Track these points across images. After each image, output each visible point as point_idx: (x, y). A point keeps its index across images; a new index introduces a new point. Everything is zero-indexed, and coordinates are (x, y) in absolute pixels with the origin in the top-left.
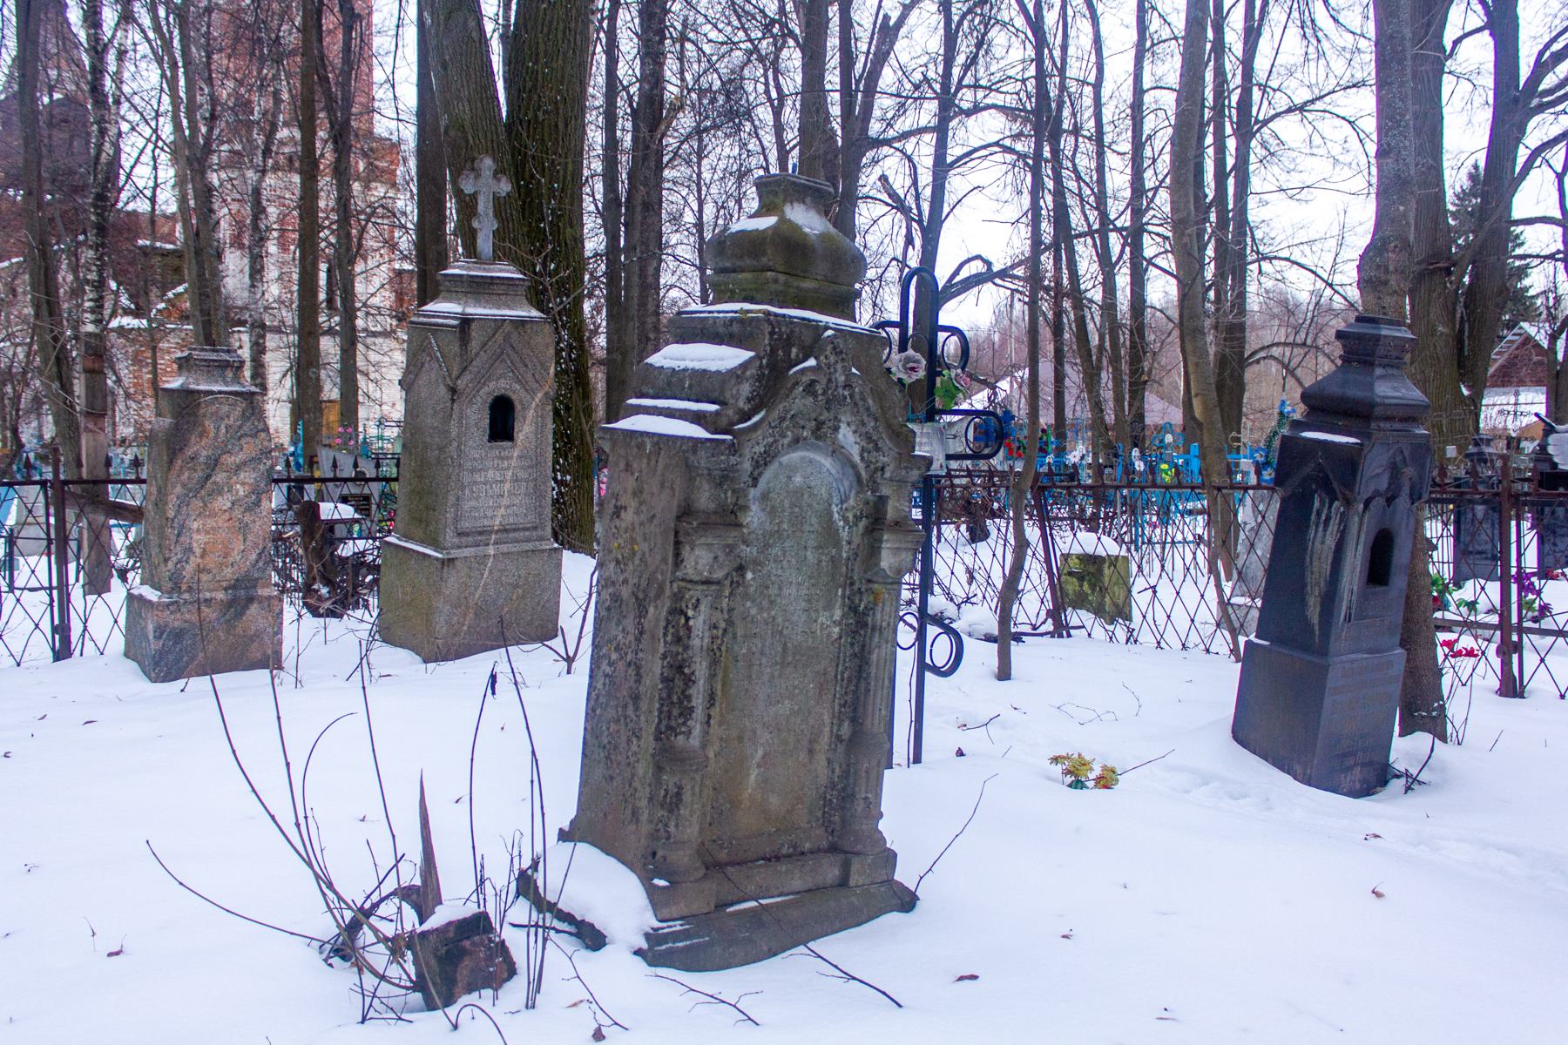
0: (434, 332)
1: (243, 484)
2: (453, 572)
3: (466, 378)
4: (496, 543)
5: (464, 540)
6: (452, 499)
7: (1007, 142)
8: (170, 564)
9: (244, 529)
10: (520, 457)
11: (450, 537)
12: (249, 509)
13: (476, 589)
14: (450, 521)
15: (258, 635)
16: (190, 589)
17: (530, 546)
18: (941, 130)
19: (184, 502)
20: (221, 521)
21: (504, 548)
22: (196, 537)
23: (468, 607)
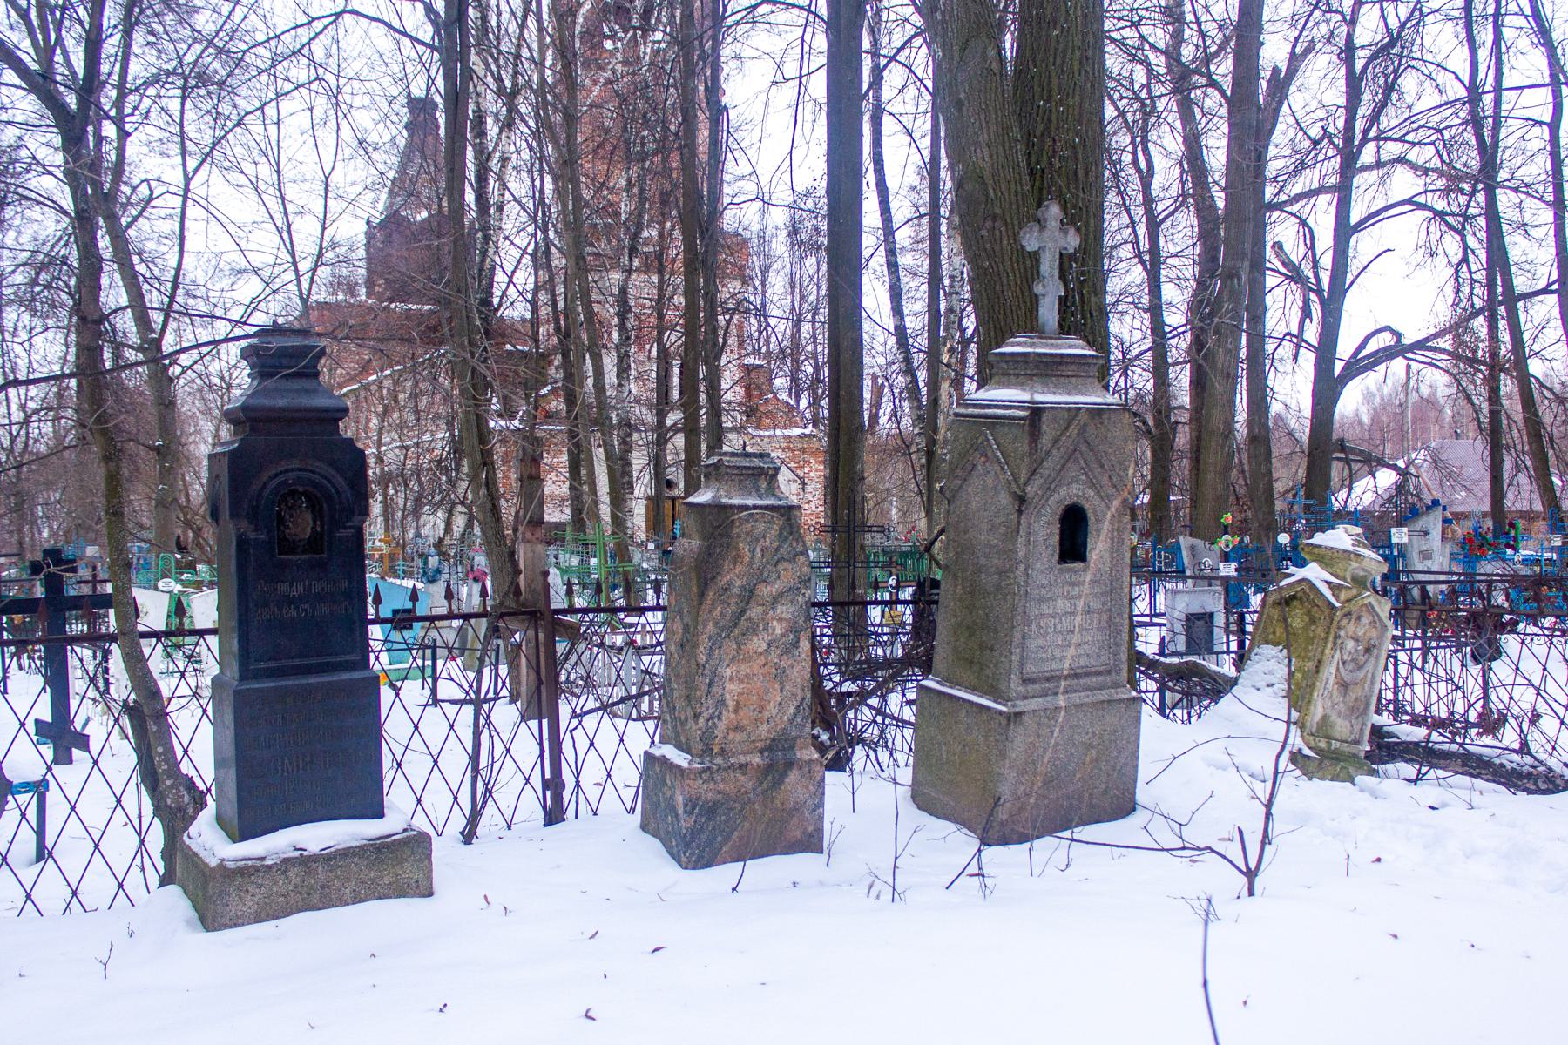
0: (992, 427)
1: (780, 620)
2: (1020, 729)
3: (1038, 482)
4: (1066, 692)
5: (1030, 687)
6: (1017, 636)
7: (1421, 199)
8: (701, 720)
9: (781, 675)
10: (1093, 582)
11: (1016, 686)
12: (785, 652)
13: (1045, 750)
14: (1015, 664)
15: (796, 809)
16: (723, 752)
17: (1103, 695)
18: (1343, 193)
19: (716, 643)
20: (756, 667)
21: (1076, 698)
22: (729, 686)
23: (1035, 774)
